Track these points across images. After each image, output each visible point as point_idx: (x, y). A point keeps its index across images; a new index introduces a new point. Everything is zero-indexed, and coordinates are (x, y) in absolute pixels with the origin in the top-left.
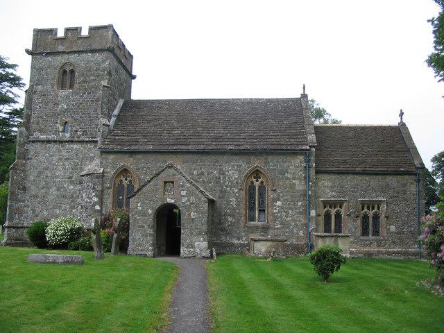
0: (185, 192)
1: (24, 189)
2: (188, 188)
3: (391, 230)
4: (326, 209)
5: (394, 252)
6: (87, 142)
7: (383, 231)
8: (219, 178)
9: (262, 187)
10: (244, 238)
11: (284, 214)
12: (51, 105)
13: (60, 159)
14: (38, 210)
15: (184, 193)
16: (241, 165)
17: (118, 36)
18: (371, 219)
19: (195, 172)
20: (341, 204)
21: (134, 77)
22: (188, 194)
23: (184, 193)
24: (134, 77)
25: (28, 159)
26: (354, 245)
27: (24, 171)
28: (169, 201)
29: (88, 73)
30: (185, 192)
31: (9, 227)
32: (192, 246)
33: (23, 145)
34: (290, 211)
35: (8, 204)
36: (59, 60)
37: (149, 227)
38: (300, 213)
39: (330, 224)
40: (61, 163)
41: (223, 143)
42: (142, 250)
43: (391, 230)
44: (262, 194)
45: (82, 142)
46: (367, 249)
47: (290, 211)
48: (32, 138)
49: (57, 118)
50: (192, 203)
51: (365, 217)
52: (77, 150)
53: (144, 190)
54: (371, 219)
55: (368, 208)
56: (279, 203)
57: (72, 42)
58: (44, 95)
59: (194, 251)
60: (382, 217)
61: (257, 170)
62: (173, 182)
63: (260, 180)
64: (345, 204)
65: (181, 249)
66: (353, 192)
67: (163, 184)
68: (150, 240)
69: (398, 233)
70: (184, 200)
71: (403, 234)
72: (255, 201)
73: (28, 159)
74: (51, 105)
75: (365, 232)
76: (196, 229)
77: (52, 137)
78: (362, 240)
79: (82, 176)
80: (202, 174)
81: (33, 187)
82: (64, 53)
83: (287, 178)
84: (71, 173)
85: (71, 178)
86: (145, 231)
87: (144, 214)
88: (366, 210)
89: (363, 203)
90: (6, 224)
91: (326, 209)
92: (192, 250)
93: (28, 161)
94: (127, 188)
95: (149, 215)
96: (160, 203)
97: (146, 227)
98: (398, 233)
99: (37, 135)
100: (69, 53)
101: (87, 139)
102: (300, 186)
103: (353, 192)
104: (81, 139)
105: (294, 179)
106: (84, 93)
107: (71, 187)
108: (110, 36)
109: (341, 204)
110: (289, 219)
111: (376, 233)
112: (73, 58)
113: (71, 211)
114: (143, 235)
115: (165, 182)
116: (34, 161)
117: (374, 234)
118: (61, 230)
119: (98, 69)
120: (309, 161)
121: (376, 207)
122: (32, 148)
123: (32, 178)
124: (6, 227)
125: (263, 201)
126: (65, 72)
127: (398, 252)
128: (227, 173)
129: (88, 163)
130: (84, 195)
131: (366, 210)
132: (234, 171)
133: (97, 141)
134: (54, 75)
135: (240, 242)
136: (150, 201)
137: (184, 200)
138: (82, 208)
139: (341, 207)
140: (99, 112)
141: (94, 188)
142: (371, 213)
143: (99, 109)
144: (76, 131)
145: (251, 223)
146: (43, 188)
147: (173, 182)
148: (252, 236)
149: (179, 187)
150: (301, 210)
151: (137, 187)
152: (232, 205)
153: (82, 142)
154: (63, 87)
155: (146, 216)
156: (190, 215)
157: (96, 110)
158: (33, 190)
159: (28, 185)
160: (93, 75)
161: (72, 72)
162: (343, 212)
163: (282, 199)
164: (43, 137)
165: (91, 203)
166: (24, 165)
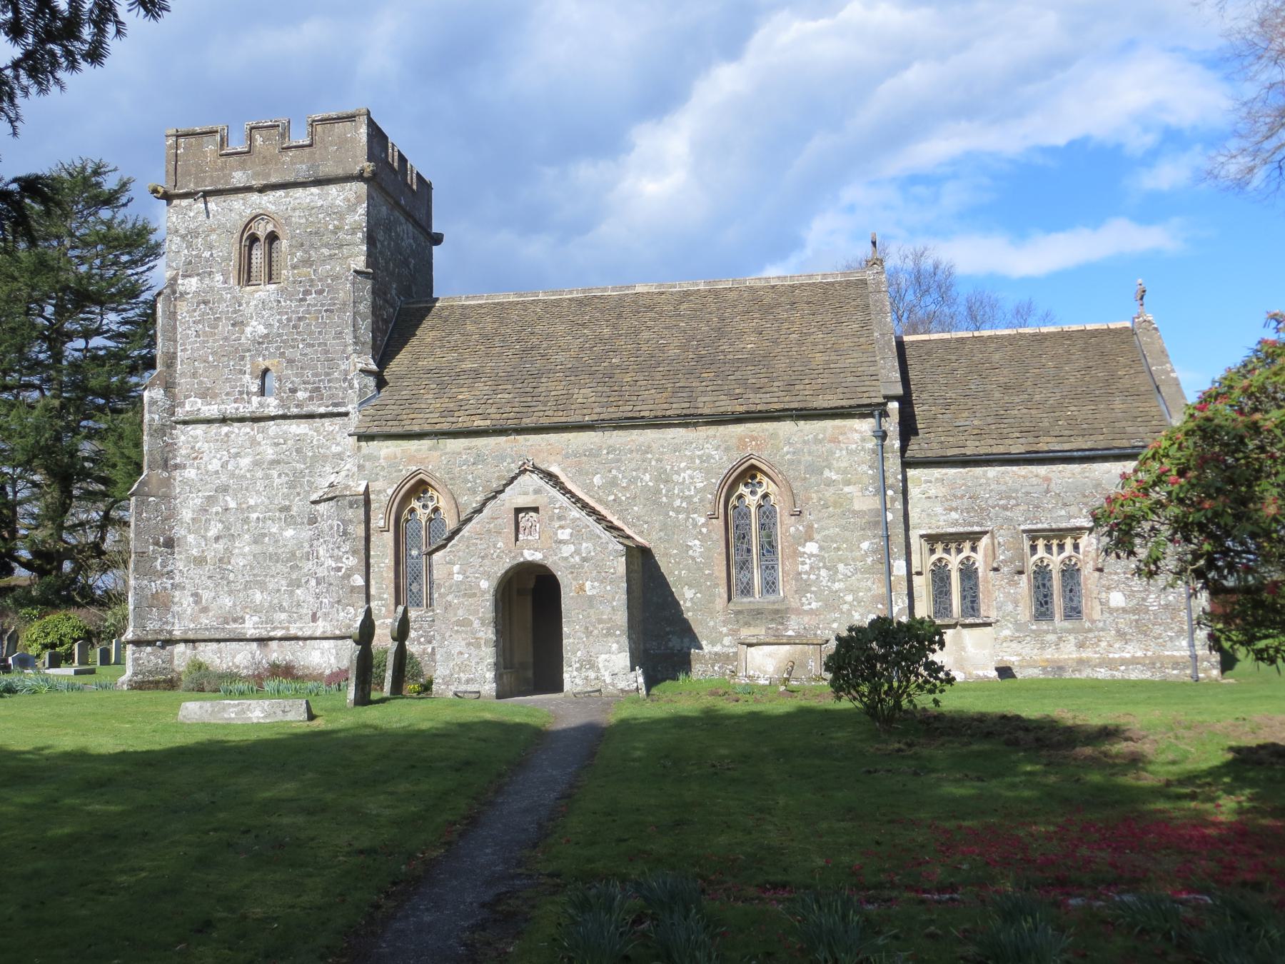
0: (569, 531)
1: (170, 544)
2: (574, 520)
3: (1113, 604)
4: (935, 557)
5: (1124, 662)
6: (322, 416)
7: (1092, 609)
8: (659, 491)
9: (767, 513)
10: (727, 641)
11: (823, 572)
12: (224, 327)
13: (256, 464)
14: (206, 595)
15: (564, 534)
16: (710, 457)
17: (386, 138)
18: (1056, 577)
19: (597, 480)
20: (974, 537)
21: (438, 239)
22: (577, 536)
23: (564, 534)
24: (438, 239)
25: (176, 467)
26: (1014, 645)
27: (167, 497)
28: (530, 556)
29: (315, 239)
30: (569, 531)
31: (138, 643)
32: (592, 666)
33: (162, 431)
34: (841, 567)
35: (132, 582)
36: (241, 208)
37: (483, 624)
38: (869, 570)
39: (948, 593)
40: (260, 474)
41: (899, 567)
42: (468, 681)
43: (1113, 604)
44: (767, 525)
45: (311, 416)
46: (1049, 654)
47: (841, 567)
48: (180, 413)
49: (242, 358)
50: (584, 560)
51: (1042, 573)
52: (299, 439)
53: (466, 531)
54: (1056, 577)
55: (1048, 548)
56: (811, 548)
57: (266, 161)
58: (205, 303)
59: (597, 678)
60: (1087, 571)
61: (753, 467)
62: (536, 510)
63: (760, 492)
64: (985, 540)
65: (566, 676)
66: (1005, 508)
67: (512, 516)
68: (488, 655)
69: (1134, 611)
70: (567, 550)
71: (1147, 612)
72: (747, 540)
73: (176, 467)
74: (224, 327)
75: (1043, 608)
76: (600, 621)
77: (230, 409)
78: (1033, 631)
79: (314, 502)
80: (613, 483)
81: (191, 538)
82: (248, 189)
83: (830, 483)
84: (286, 497)
85: (286, 509)
86: (474, 633)
87: (468, 591)
88: (1041, 552)
89: (1034, 535)
90: (129, 635)
91: (935, 557)
92: (592, 675)
93: (177, 473)
94: (428, 529)
95: (484, 592)
96: (507, 563)
97: (476, 624)
98: (1134, 611)
99: (192, 405)
100: (262, 190)
101: (322, 410)
102: (865, 502)
103: (1005, 508)
104: (305, 410)
105: (848, 483)
106: (307, 293)
107: (289, 533)
108: (364, 139)
109: (974, 537)
110: (837, 586)
111: (1073, 612)
112: (268, 202)
113: (292, 593)
114: (469, 644)
115: (518, 511)
116: (190, 473)
117: (1067, 617)
118: (244, 555)
119: (337, 229)
120: (883, 436)
121: (1069, 542)
122: (183, 436)
123: (187, 515)
124: (129, 642)
125: (770, 543)
126: (254, 239)
127: (1134, 661)
128: (675, 477)
129: (328, 469)
130: (321, 552)
131: (1041, 552)
132: (694, 460)
133: (346, 414)
134: (227, 249)
135: (718, 648)
136: (483, 558)
137: (567, 550)
138: (318, 583)
139: (974, 549)
140: (349, 339)
141: (345, 533)
142: (1055, 561)
143: (349, 331)
144: (293, 391)
145: (745, 600)
146: (217, 539)
147: (536, 510)
148: (745, 633)
149: (551, 519)
150: (869, 560)
151: (451, 524)
152: (693, 558)
153: (311, 416)
154: (246, 275)
155: (474, 595)
156: (582, 588)
157: (339, 335)
158: (191, 542)
159: (179, 532)
160: (327, 245)
161: (272, 238)
162: (979, 559)
163: (817, 536)
164: (211, 410)
165: (339, 569)
166: (167, 483)
